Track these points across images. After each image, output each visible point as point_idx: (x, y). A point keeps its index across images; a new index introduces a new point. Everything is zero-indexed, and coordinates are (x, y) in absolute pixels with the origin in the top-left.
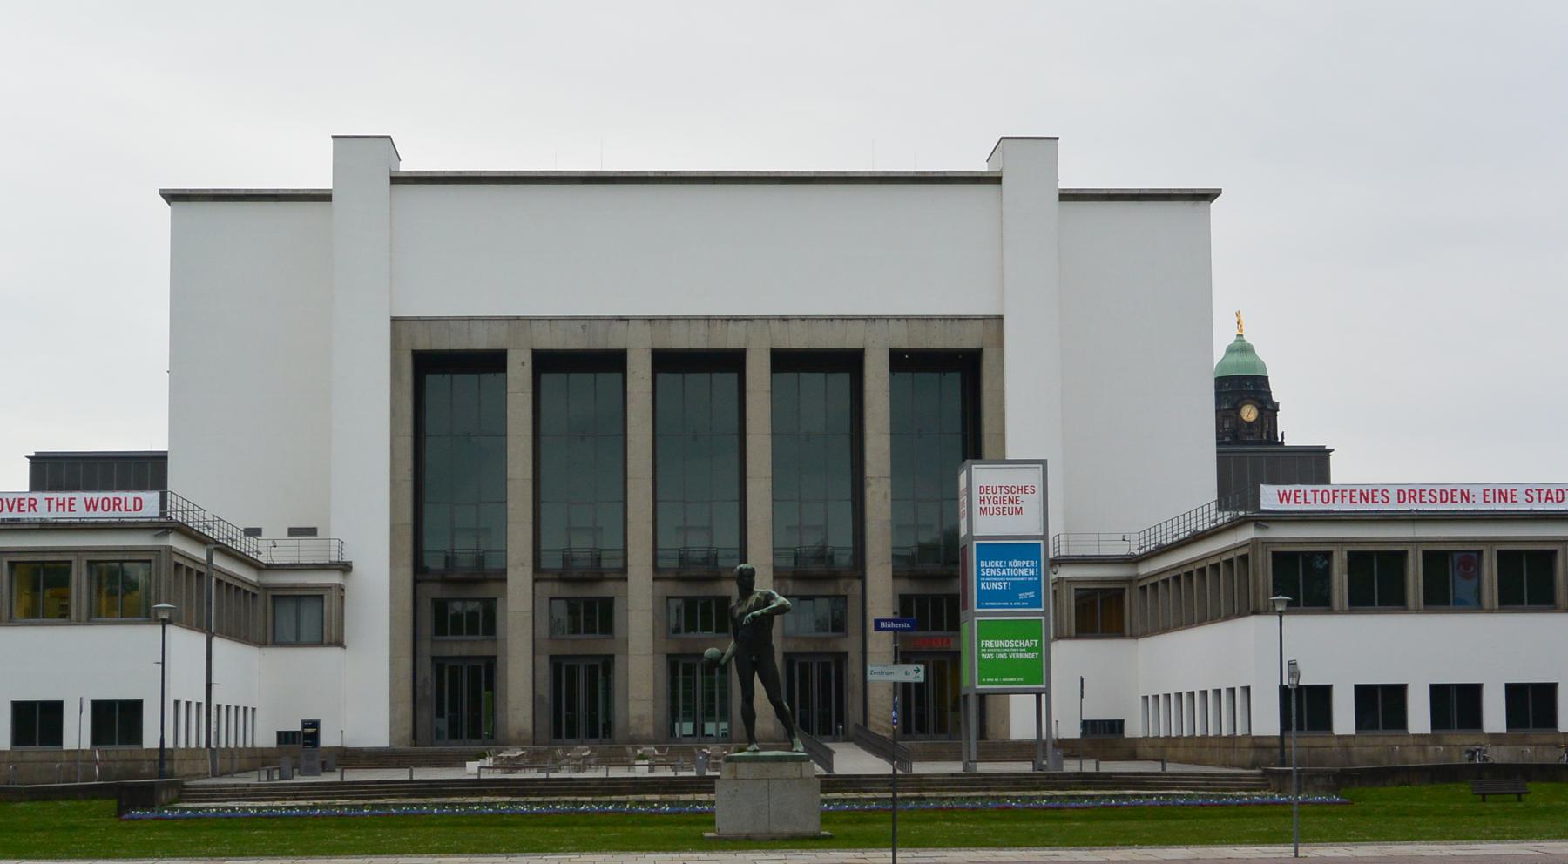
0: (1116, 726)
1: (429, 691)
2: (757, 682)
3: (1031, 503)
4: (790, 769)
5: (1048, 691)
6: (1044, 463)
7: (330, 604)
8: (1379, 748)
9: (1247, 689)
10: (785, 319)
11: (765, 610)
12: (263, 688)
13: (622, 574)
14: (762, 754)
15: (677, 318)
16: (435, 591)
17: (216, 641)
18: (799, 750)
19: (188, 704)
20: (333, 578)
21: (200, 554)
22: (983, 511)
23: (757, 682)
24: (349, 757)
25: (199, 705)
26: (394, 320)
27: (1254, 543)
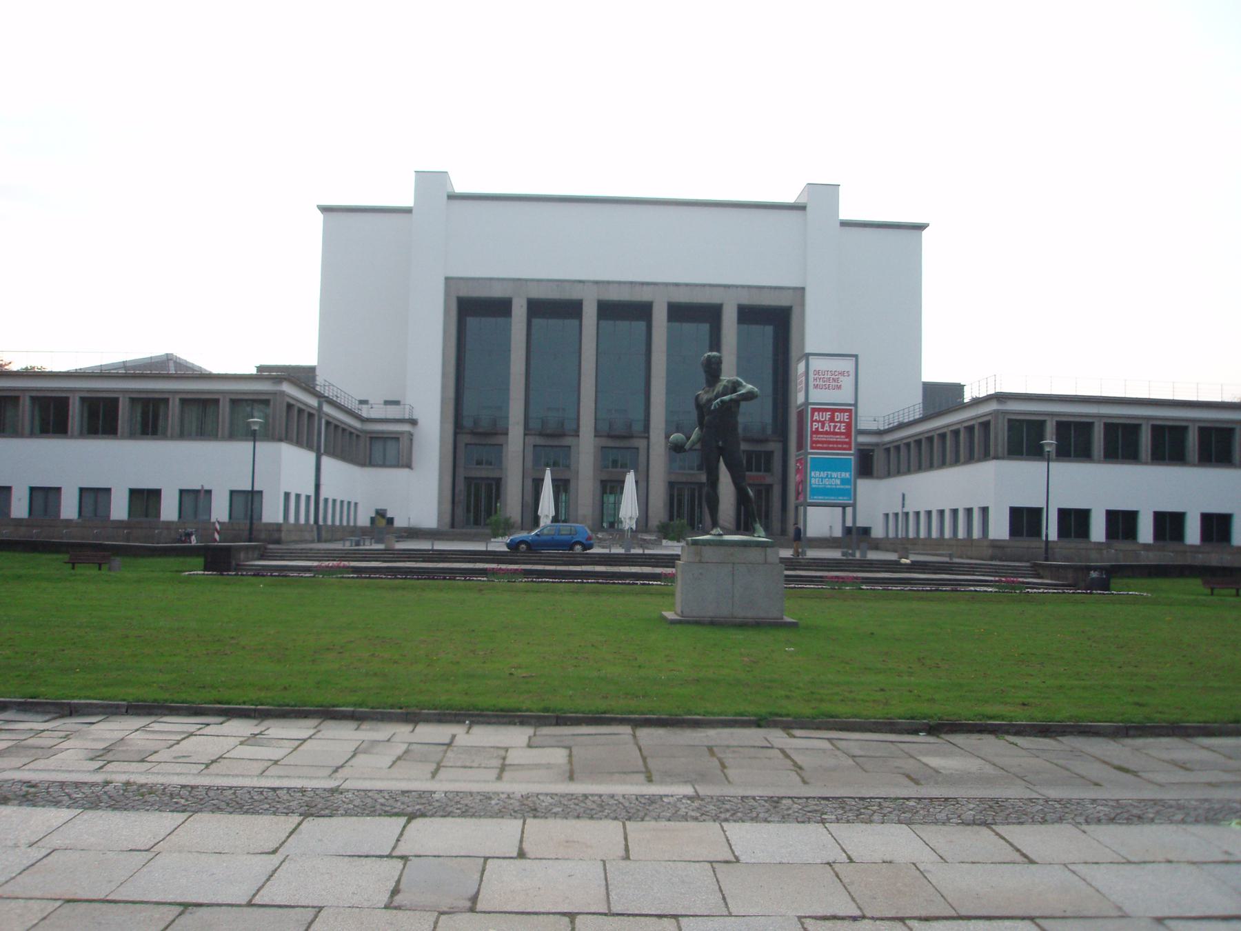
0: (866, 531)
1: (462, 497)
2: (723, 468)
3: (847, 383)
4: (754, 555)
5: (854, 506)
6: (856, 356)
7: (404, 441)
8: (1120, 553)
9: (985, 511)
10: (677, 285)
11: (734, 396)
12: (352, 487)
13: (576, 434)
14: (727, 537)
15: (613, 282)
16: (465, 439)
17: (326, 461)
18: (760, 536)
19: (334, 501)
20: (406, 428)
21: (313, 402)
22: (816, 387)
23: (723, 468)
24: (413, 533)
25: (308, 497)
26: (447, 279)
27: (996, 412)
